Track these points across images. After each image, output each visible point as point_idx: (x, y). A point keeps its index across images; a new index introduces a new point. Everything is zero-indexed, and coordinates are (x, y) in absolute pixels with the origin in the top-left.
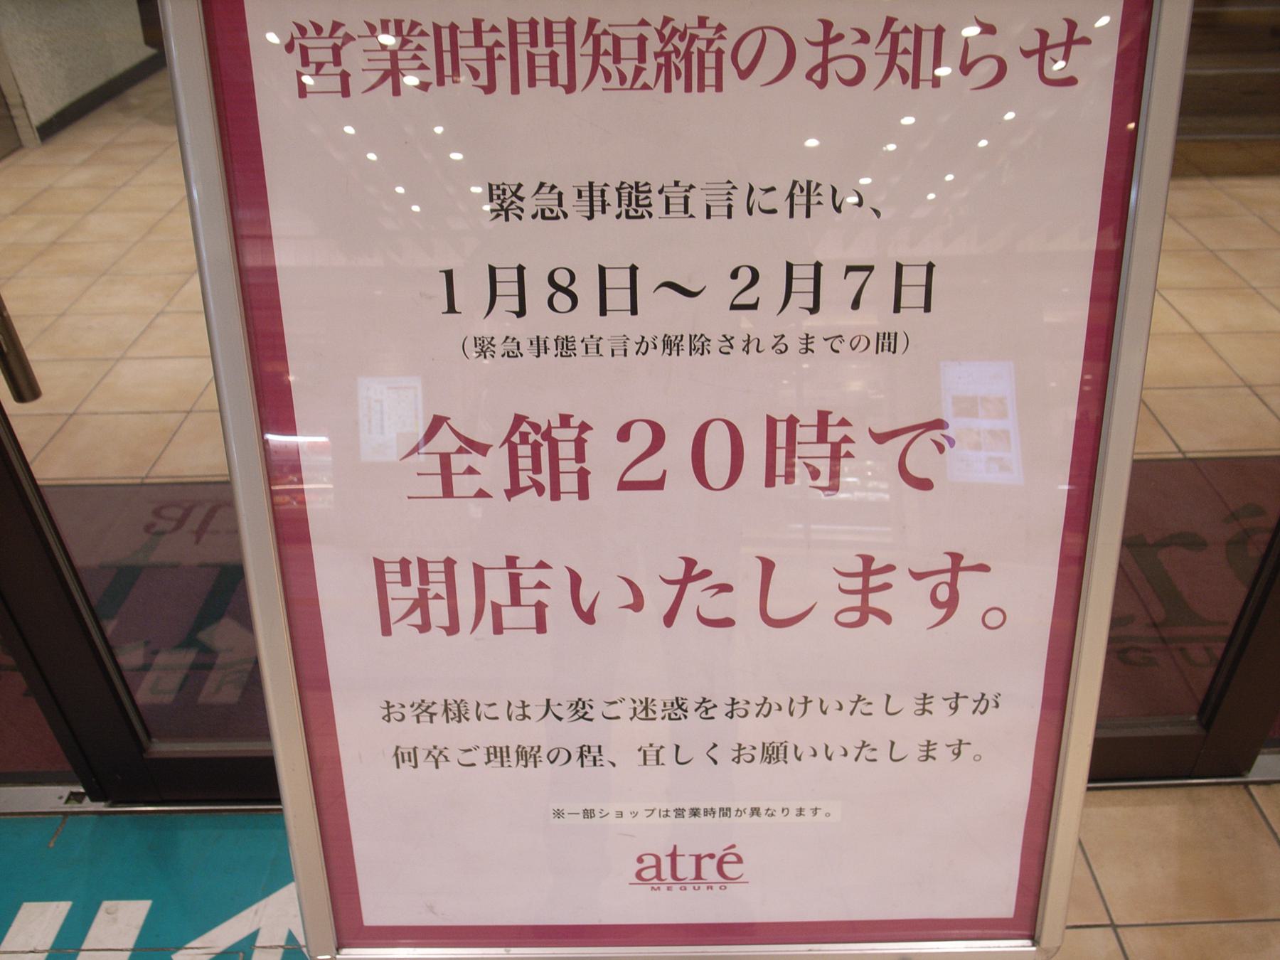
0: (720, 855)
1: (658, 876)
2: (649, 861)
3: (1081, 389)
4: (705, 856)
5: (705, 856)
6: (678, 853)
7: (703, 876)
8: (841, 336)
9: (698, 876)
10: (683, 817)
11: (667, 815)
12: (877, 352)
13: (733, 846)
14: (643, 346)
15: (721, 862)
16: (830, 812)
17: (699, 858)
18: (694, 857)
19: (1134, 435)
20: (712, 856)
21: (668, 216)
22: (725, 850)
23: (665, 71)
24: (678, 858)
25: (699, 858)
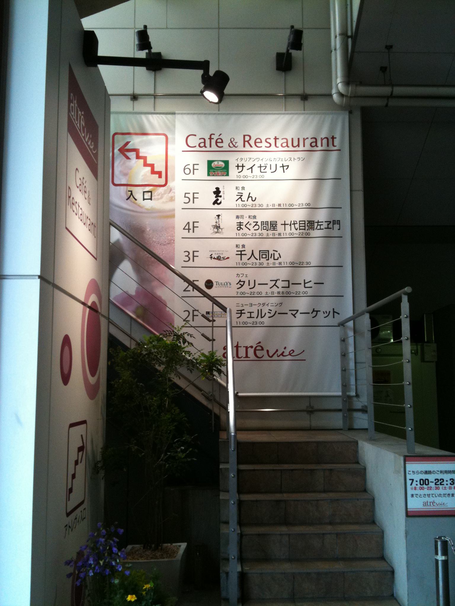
0: (255, 346)
1: (426, 505)
2: (425, 503)
3: (220, 176)
4: (249, 347)
5: (249, 347)
6: (239, 346)
7: (249, 356)
8: (280, 257)
9: (247, 356)
10: (242, 248)
11: (240, 228)
12: (277, 230)
13: (260, 343)
14: (215, 251)
15: (255, 350)
16: (244, 186)
17: (247, 348)
18: (245, 348)
19: (58, 129)
20: (252, 347)
21: (217, 235)
22: (257, 344)
23: (172, 265)
24: (239, 348)
25: (247, 348)
